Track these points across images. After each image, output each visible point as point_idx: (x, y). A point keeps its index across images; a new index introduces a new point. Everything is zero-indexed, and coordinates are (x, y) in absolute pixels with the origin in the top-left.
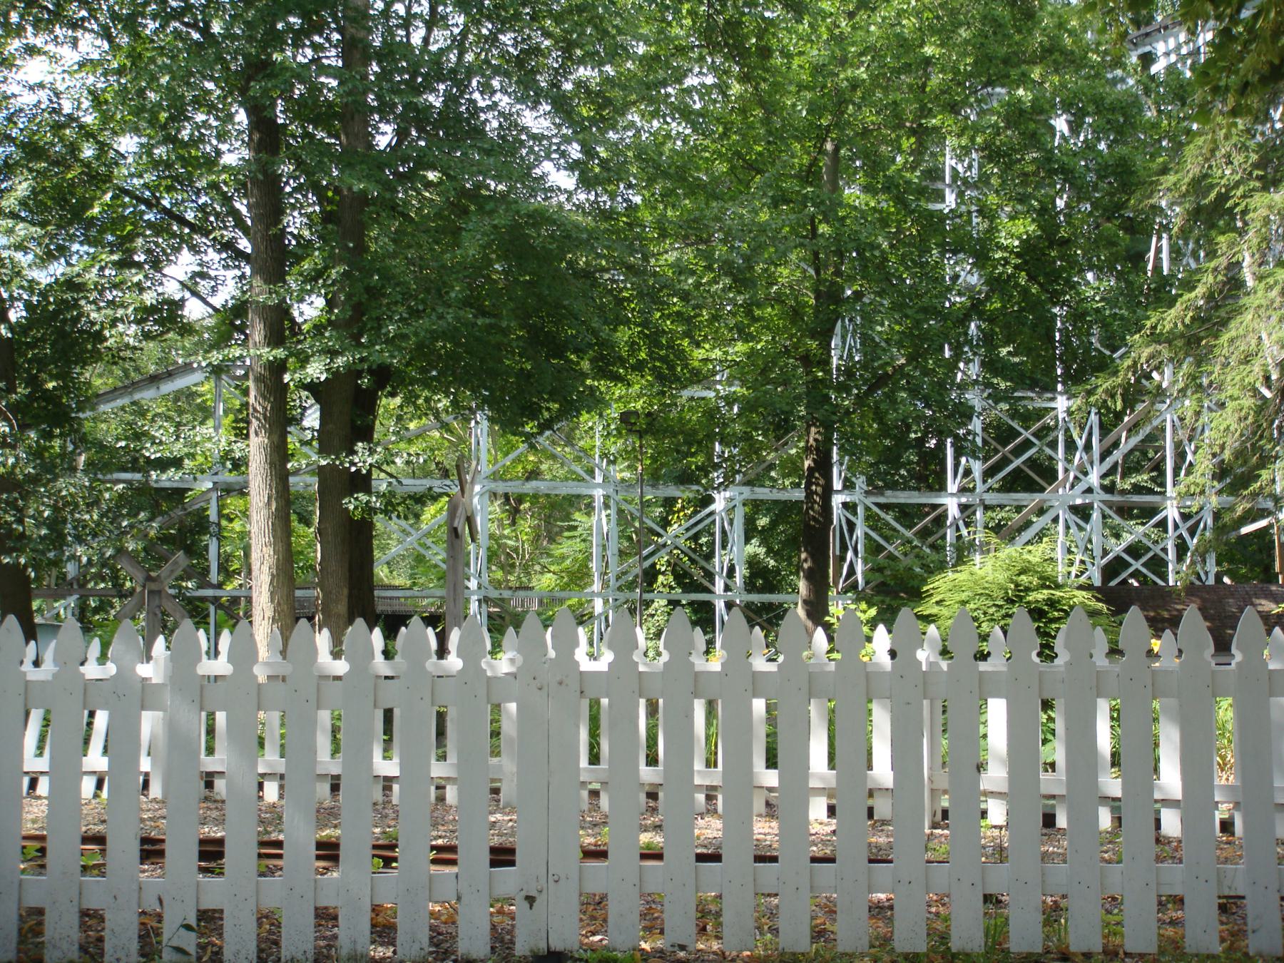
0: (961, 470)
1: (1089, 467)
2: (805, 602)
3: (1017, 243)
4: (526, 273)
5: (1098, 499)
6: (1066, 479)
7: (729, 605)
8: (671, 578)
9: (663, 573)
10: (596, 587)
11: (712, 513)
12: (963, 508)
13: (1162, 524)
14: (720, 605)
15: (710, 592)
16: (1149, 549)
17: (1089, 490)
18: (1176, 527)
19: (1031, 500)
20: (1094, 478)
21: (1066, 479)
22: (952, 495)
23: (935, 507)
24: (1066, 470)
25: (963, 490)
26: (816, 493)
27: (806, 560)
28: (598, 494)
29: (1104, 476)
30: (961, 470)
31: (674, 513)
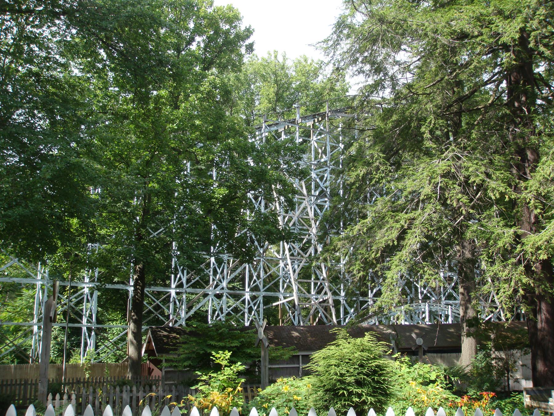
0: (177, 279)
1: (222, 280)
2: (133, 332)
3: (221, 196)
4: (20, 192)
5: (225, 292)
6: (213, 284)
7: (89, 330)
8: (62, 317)
9: (59, 315)
10: (35, 320)
11: (82, 294)
12: (177, 294)
13: (244, 302)
14: (84, 329)
15: (79, 322)
16: (242, 310)
17: (223, 288)
18: (249, 304)
19: (201, 291)
20: (224, 284)
21: (213, 284)
22: (173, 289)
23: (168, 292)
24: (214, 280)
25: (177, 287)
26: (139, 289)
27: (134, 316)
28: (39, 283)
29: (230, 282)
30: (177, 279)
31: (65, 291)
